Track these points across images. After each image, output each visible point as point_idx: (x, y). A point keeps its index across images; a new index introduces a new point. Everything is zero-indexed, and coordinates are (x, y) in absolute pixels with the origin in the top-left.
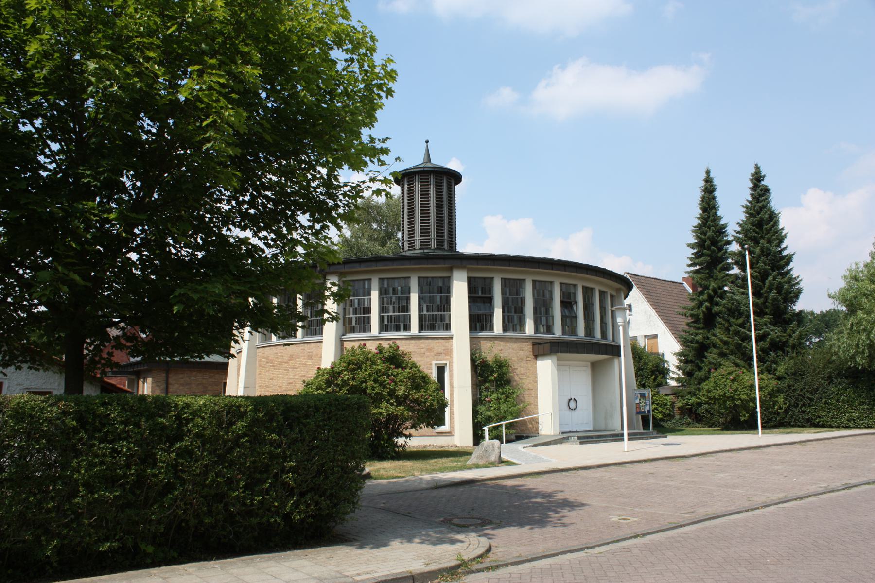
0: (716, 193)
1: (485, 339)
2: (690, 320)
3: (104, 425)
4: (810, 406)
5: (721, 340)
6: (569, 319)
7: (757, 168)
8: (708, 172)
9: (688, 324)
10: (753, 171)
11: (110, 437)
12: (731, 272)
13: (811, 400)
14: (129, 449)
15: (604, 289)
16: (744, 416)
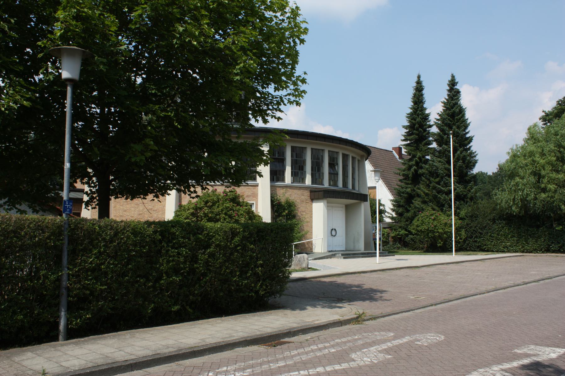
0: (424, 92)
1: (280, 187)
2: (401, 178)
3: (173, 239)
4: (480, 238)
5: (424, 193)
6: (333, 175)
7: (453, 76)
8: (419, 77)
9: (400, 181)
10: (450, 78)
11: (176, 246)
12: (431, 146)
13: (481, 234)
14: (186, 252)
15: (355, 156)
16: (440, 243)
